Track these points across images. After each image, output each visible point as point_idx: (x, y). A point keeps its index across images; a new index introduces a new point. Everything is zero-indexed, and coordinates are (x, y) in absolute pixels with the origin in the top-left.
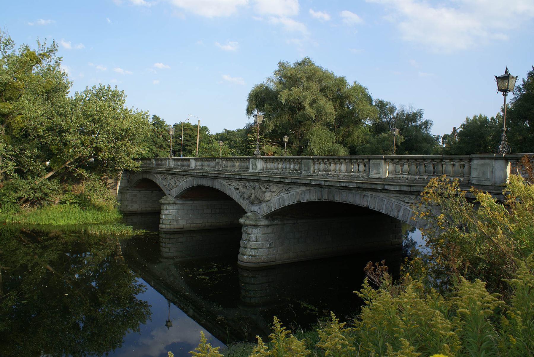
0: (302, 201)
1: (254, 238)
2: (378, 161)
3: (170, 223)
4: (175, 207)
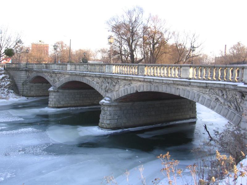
0: (139, 91)
1: (108, 113)
2: (187, 68)
3: (55, 103)
4: (58, 94)
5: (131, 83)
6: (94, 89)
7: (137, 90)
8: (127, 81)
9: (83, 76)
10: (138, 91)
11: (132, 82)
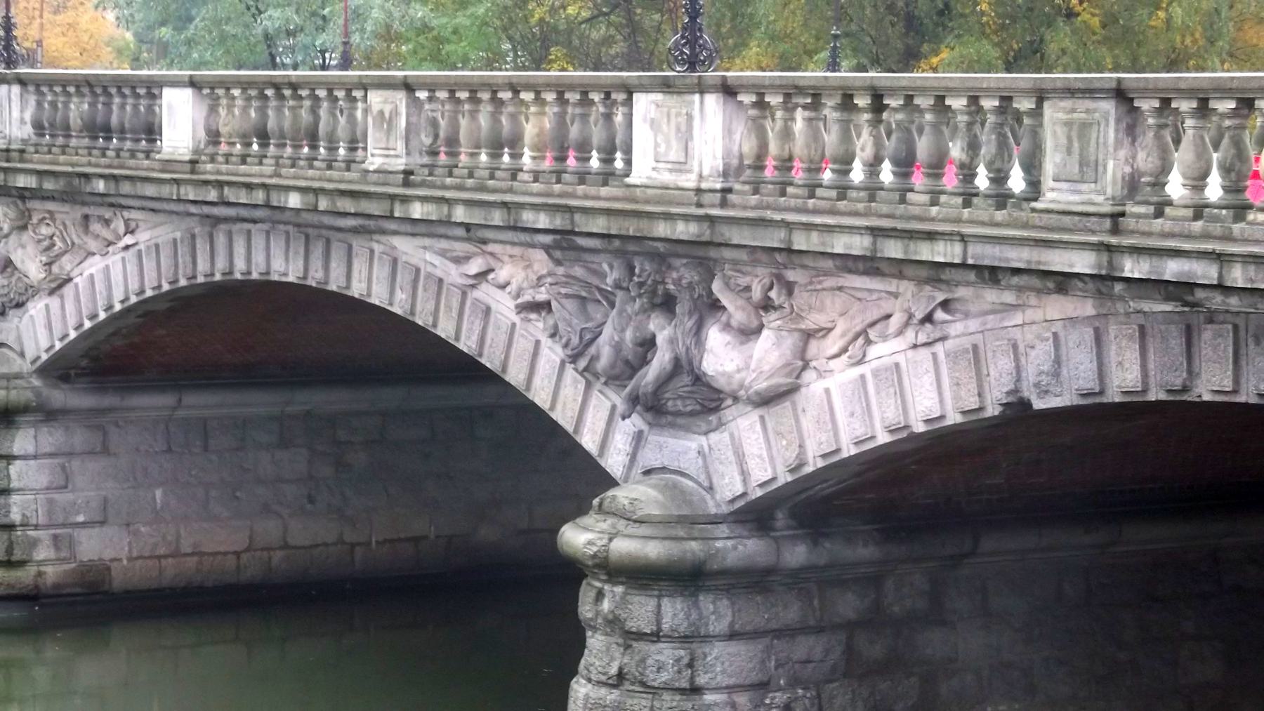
0: (1038, 404)
5: (945, 305)
6: (491, 378)
7: (1015, 391)
8: (901, 276)
9: (355, 231)
10: (1025, 404)
11: (961, 292)
